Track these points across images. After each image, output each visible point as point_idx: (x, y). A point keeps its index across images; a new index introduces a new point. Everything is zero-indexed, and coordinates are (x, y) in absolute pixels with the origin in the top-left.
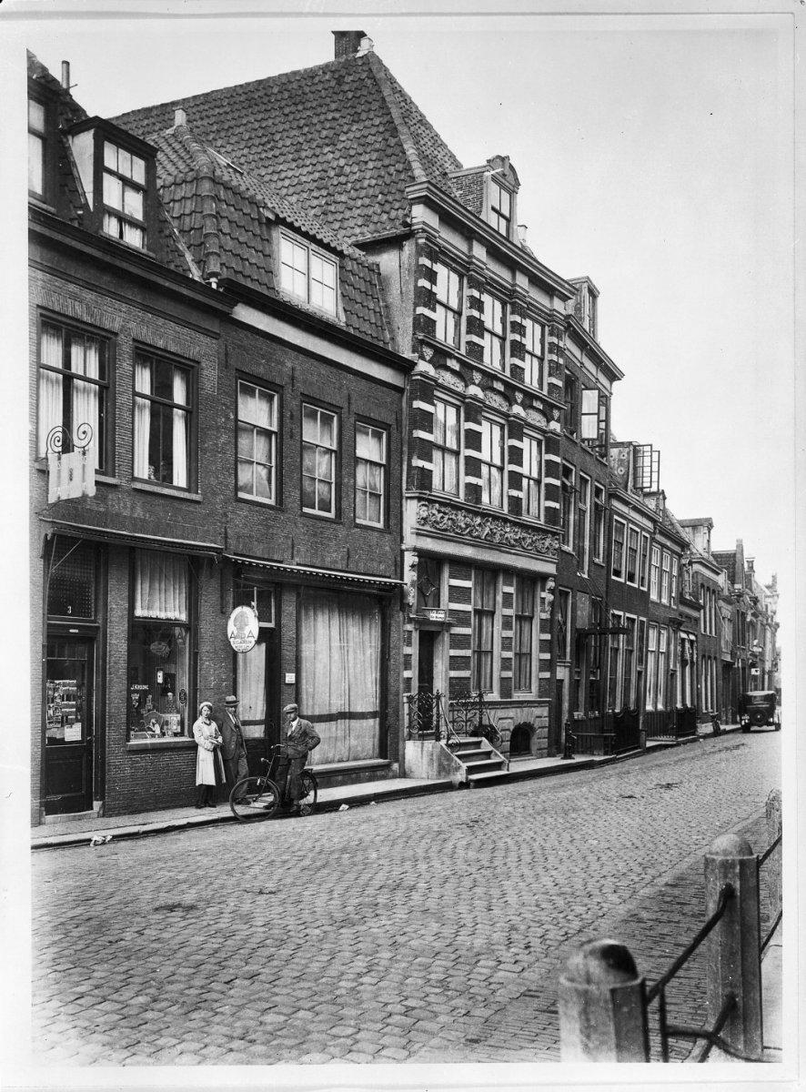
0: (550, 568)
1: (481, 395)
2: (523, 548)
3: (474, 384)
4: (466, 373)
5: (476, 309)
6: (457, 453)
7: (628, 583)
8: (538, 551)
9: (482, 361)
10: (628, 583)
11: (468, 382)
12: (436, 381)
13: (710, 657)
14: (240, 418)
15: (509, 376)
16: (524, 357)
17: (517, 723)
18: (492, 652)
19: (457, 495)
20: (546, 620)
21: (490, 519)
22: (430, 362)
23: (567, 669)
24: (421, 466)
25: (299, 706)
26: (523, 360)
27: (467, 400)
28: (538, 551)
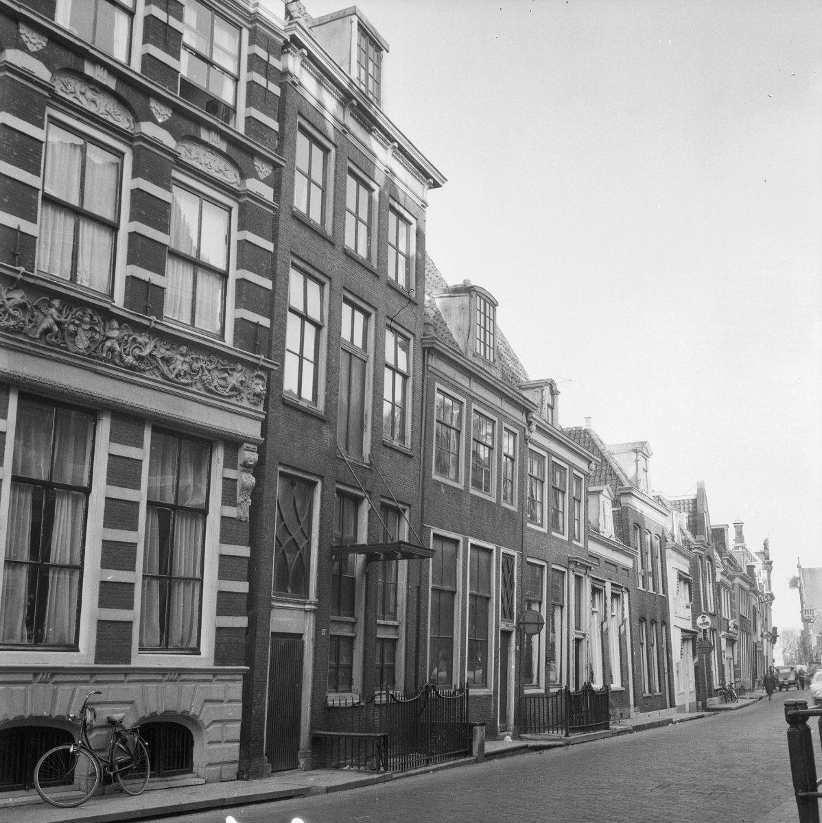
0: (250, 429)
1: (41, 71)
2: (163, 375)
3: (257, 178)
4: (135, 99)
5: (261, 74)
6: (113, 228)
7: (473, 491)
8: (210, 391)
9: (53, 19)
10: (473, 491)
11: (139, 115)
12: (51, 91)
13: (653, 622)
14: (304, 356)
15: (138, 70)
16: (179, 53)
17: (142, 713)
18: (201, 580)
19: (222, 336)
20: (238, 520)
21: (56, 303)
22: (265, 181)
23: (311, 617)
24: (256, 321)
25: (252, 667)
26: (178, 59)
27: (136, 144)
28: (210, 391)
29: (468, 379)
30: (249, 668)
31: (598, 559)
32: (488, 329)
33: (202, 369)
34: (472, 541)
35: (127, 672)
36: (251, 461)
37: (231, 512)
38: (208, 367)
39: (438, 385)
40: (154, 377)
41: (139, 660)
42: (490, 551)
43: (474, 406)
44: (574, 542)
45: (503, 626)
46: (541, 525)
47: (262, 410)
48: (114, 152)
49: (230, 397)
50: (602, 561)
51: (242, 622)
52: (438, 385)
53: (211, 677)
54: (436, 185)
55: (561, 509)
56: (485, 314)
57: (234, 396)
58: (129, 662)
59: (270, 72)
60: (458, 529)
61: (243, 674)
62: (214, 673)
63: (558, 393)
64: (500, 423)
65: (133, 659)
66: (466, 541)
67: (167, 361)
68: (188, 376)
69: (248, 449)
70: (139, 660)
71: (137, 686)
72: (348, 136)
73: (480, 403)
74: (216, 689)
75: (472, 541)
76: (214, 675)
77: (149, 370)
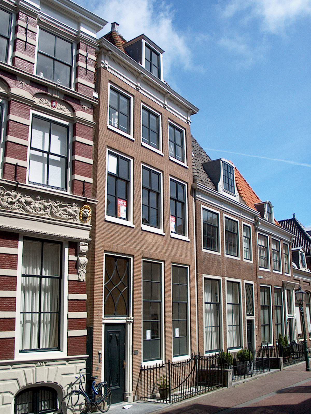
29: (186, 114)
30: (88, 356)
31: (309, 283)
32: (230, 177)
33: (51, 207)
34: (227, 279)
35: (11, 364)
36: (85, 251)
37: (74, 277)
38: (55, 205)
39: (202, 206)
40: (21, 212)
41: (18, 357)
42: (239, 283)
43: (225, 215)
44: (286, 274)
45: (248, 318)
46: (127, 219)
47: (89, 225)
48: (2, 111)
49: (69, 219)
50: (302, 281)
51: (84, 332)
52: (202, 206)
53: (65, 362)
54: (194, 113)
55: (304, 260)
56: (228, 184)
57: (72, 219)
58: (13, 358)
59: (88, 61)
60: (219, 274)
61: (86, 360)
62: (67, 360)
63: (273, 207)
64: (240, 222)
65: (15, 358)
66: (224, 280)
67: (28, 203)
68: (42, 210)
69: (82, 245)
70: (18, 357)
71: (21, 370)
72: (140, 91)
73: (227, 213)
74: (69, 367)
75: (227, 279)
76: (67, 362)
77: (18, 209)
